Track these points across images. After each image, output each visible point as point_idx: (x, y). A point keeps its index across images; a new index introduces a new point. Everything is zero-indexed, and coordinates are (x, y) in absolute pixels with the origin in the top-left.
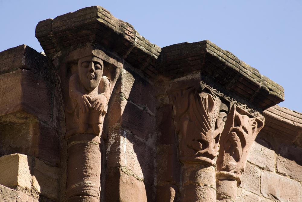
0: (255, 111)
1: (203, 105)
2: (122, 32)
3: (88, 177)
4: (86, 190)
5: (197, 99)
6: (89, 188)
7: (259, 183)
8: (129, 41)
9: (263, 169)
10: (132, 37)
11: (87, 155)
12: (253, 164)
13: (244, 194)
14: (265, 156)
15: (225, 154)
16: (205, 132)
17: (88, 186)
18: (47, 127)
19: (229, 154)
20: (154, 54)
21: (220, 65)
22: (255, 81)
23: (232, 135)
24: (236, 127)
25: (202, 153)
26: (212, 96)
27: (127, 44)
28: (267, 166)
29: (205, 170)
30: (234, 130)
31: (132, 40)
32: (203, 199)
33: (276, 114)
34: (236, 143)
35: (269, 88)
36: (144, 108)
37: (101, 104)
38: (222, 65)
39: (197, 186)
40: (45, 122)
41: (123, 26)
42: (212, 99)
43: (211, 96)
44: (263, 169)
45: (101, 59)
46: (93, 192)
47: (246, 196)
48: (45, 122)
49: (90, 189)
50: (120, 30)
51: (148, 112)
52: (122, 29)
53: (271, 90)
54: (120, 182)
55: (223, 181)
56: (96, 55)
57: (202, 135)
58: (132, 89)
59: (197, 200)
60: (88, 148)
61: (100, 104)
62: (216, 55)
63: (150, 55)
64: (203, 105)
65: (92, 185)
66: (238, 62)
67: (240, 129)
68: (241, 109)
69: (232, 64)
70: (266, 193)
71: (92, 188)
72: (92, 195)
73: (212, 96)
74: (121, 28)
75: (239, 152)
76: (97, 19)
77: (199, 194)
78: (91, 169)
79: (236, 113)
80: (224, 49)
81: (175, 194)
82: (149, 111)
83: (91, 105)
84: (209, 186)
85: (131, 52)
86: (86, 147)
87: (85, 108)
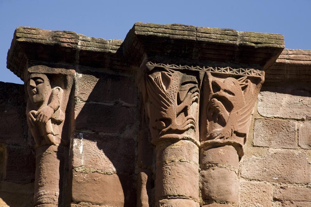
0: (246, 69)
1: (157, 84)
2: (56, 42)
3: (42, 187)
4: (40, 199)
5: (149, 81)
6: (43, 196)
7: (297, 136)
8: (69, 48)
9: (303, 120)
10: (72, 43)
11: (41, 166)
12: (286, 119)
13: (272, 152)
14: (305, 106)
15: (208, 123)
16: (165, 109)
17: (42, 195)
18: (18, 149)
19: (213, 122)
20: (110, 49)
21: (163, 41)
22: (226, 41)
23: (212, 103)
24: (215, 93)
25: (165, 131)
26: (166, 73)
27: (69, 51)
28: (307, 116)
29: (171, 147)
30: (215, 96)
31: (73, 46)
32: (169, 176)
33: (306, 60)
34: (217, 109)
35: (254, 43)
36: (117, 103)
37: (44, 116)
38: (166, 40)
39: (164, 164)
40: (16, 145)
41: (57, 36)
42: (168, 75)
43: (164, 73)
44: (303, 120)
45: (42, 73)
46: (46, 199)
47: (274, 155)
48: (16, 145)
49: (43, 198)
50: (53, 41)
51: (123, 105)
52: (56, 39)
53: (256, 43)
54: (73, 183)
55: (208, 150)
56: (32, 72)
57: (162, 113)
58: (94, 90)
59: (163, 179)
60: (43, 160)
61: (43, 115)
62: (152, 33)
63: (105, 52)
64: (157, 84)
65: (46, 193)
66: (191, 30)
67: (222, 93)
68: (219, 74)
69: (182, 35)
70: (305, 144)
71: (45, 196)
72: (46, 203)
73: (166, 73)
74: (55, 38)
75: (223, 117)
76: (17, 40)
77: (166, 172)
78: (45, 178)
79: (211, 79)
80: (168, 23)
81: (147, 178)
82: (125, 104)
83: (35, 119)
84: (177, 160)
85: (80, 56)
86: (41, 159)
87: (31, 123)
